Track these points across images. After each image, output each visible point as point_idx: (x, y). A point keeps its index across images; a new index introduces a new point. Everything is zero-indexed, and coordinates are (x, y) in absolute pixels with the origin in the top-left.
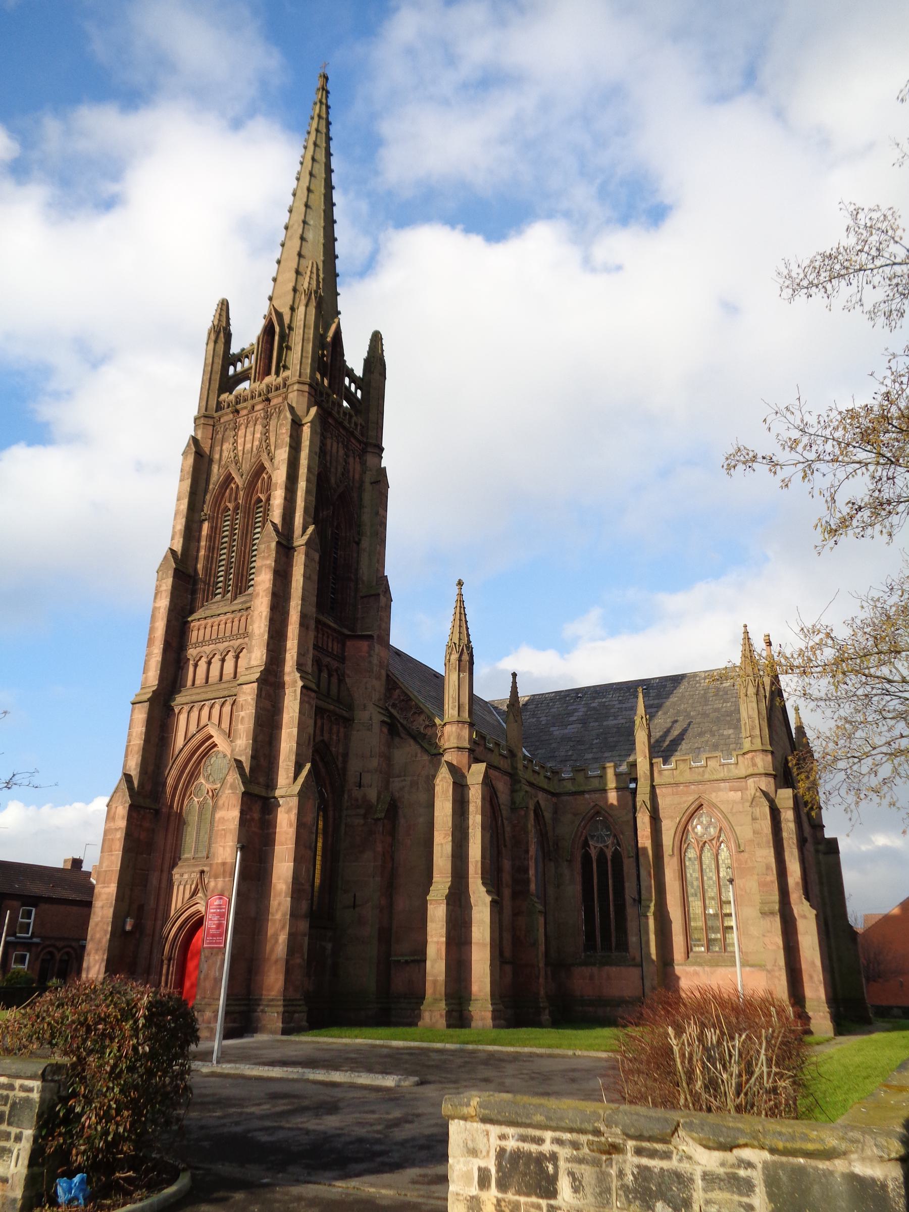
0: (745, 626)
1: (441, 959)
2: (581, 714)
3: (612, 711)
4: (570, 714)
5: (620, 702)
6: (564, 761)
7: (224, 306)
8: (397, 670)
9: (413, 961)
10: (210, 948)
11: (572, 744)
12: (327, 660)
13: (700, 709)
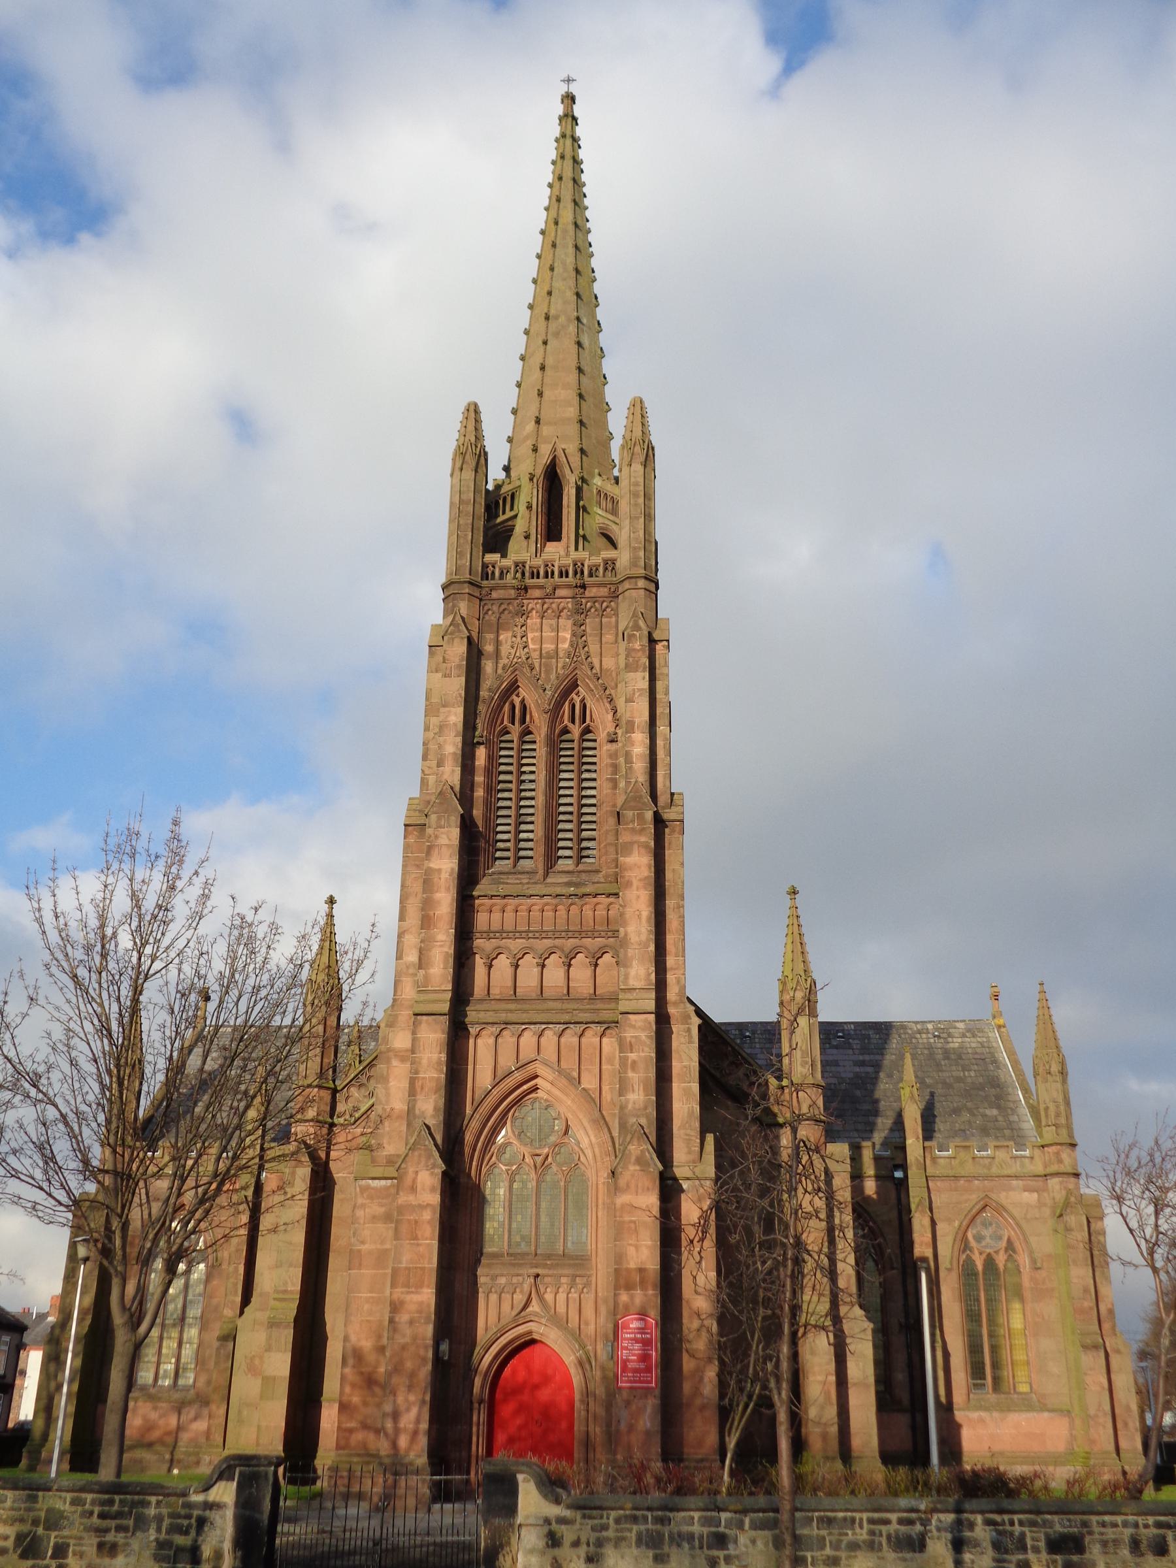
1: (831, 1404)
7: (473, 413)
10: (631, 1388)
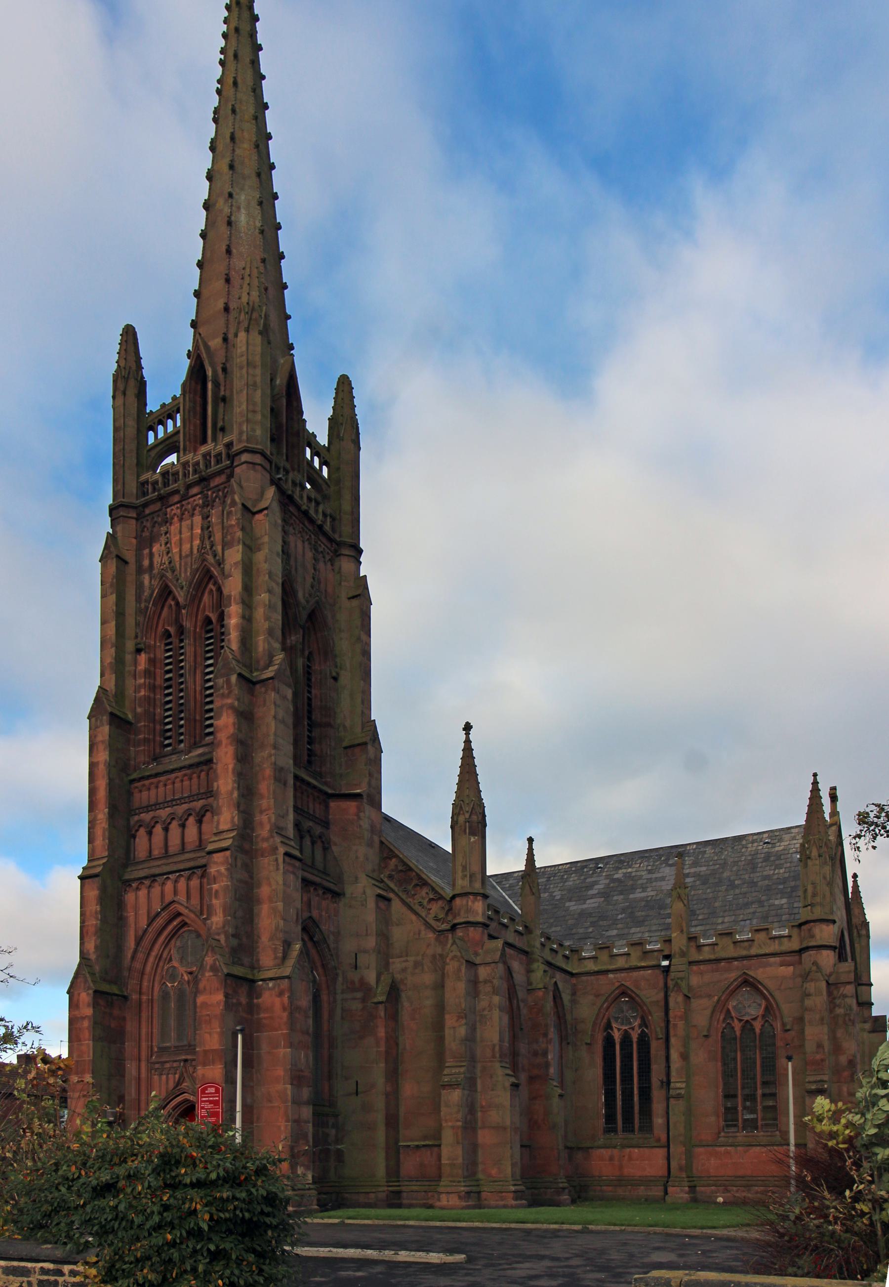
0: (815, 775)
2: (601, 886)
3: (640, 882)
4: (591, 886)
5: (650, 872)
6: (585, 937)
7: (129, 336)
8: (390, 837)
9: (424, 1146)
11: (592, 919)
12: (307, 824)
13: (746, 877)
